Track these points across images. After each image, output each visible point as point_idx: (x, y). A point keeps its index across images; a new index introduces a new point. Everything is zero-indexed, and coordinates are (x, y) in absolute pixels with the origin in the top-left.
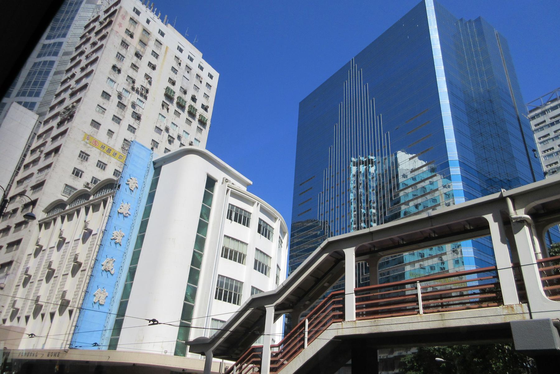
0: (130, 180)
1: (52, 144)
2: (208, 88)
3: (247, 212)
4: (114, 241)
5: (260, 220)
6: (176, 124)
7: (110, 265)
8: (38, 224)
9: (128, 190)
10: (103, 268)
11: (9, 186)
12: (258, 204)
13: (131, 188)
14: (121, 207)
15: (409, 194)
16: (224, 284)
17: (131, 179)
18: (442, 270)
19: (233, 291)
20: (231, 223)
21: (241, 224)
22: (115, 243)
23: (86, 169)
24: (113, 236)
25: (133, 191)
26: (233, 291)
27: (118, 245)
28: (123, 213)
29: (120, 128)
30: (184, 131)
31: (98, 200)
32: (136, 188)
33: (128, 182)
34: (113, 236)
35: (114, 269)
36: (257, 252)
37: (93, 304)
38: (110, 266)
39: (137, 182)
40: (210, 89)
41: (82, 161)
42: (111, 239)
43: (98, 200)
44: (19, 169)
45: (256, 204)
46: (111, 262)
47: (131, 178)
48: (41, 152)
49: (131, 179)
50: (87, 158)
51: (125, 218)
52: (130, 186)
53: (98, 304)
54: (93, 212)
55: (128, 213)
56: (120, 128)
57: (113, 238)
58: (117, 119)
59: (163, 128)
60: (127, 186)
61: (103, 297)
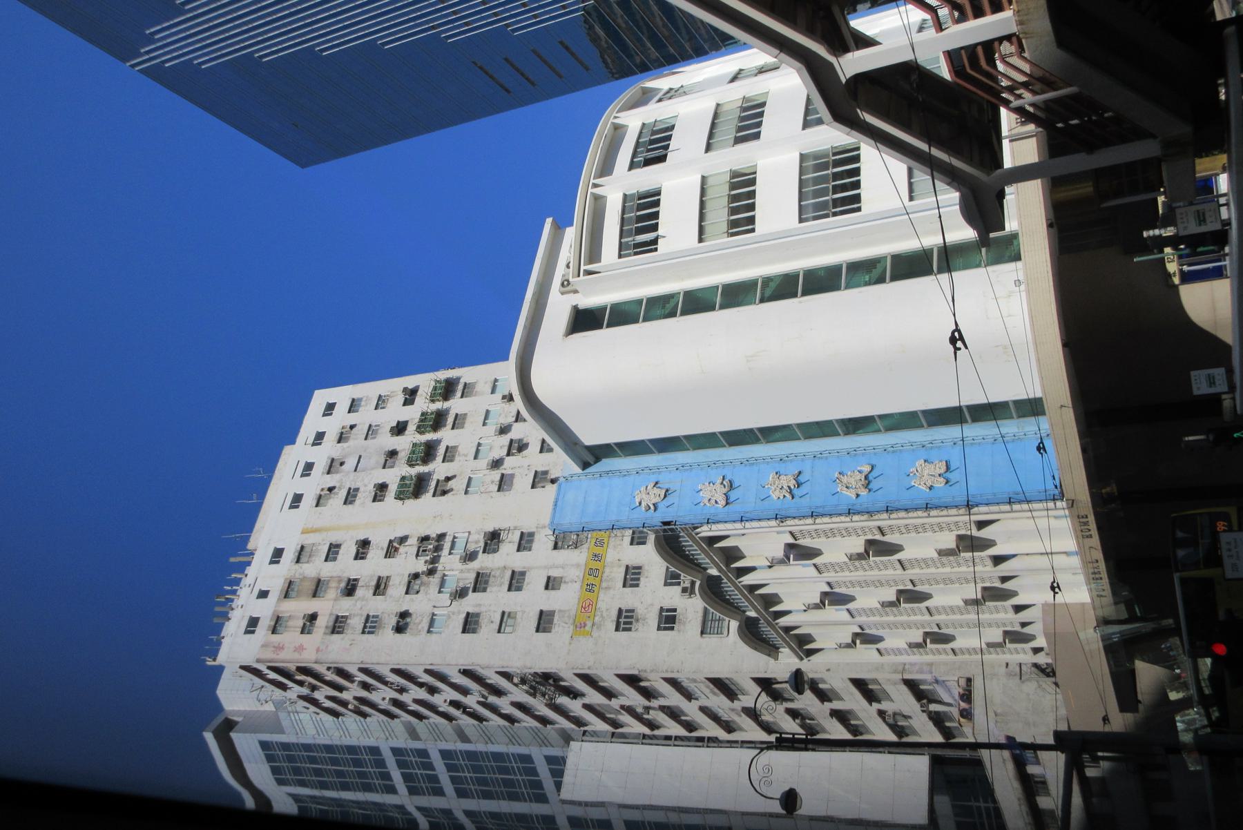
0: (643, 504)
3: (641, 133)
4: (795, 492)
5: (632, 166)
7: (852, 482)
9: (670, 500)
10: (864, 493)
12: (595, 186)
13: (662, 496)
14: (713, 502)
16: (817, 200)
17: (640, 503)
19: (829, 172)
20: (664, 237)
21: (658, 212)
22: (798, 487)
23: (652, 605)
24: (784, 496)
25: (667, 491)
26: (829, 172)
27: (801, 479)
28: (725, 494)
32: (658, 485)
33: (650, 508)
34: (784, 496)
35: (859, 468)
36: (714, 146)
37: (950, 484)
38: (855, 479)
39: (643, 489)
41: (637, 620)
42: (793, 498)
44: (700, 739)
45: (597, 191)
46: (845, 479)
47: (638, 504)
49: (640, 503)
50: (627, 611)
51: (735, 485)
52: (657, 500)
53: (948, 475)
55: (722, 483)
57: (788, 495)
59: (496, 475)
60: (661, 506)
61: (928, 470)
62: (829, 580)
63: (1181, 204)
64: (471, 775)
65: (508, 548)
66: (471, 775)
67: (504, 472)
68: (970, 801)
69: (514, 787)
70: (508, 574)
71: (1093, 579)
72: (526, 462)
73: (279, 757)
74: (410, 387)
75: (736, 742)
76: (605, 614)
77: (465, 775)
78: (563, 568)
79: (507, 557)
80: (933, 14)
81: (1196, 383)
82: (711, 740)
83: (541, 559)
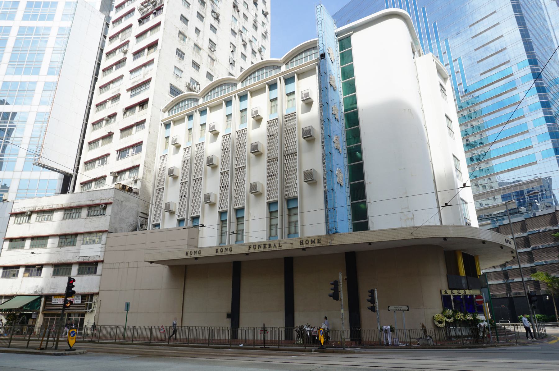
1: (137, 42)
2: (184, 22)
6: (246, 28)
8: (163, 124)
11: (91, 93)
15: (85, 217)
18: (474, 178)
23: (184, 69)
29: (204, 25)
30: (253, 36)
31: (259, 85)
40: (186, 24)
41: (180, 59)
43: (259, 85)
44: (97, 74)
48: (125, 53)
50: (183, 57)
54: (251, 97)
56: (204, 25)
58: (200, 16)
59: (236, 31)
62: (279, 101)
63: (484, 200)
64: (40, 13)
65: (212, 21)
66: (40, 13)
67: (237, 35)
68: (355, 146)
69: (35, 7)
70: (204, 15)
71: (303, 241)
72: (239, 46)
73: (4, 123)
74: (267, 16)
75: (93, 89)
76: (184, 46)
77: (41, 10)
78: (203, 39)
79: (209, 19)
80: (49, 237)
81: (275, 246)
82: (96, 79)
83: (207, 33)
